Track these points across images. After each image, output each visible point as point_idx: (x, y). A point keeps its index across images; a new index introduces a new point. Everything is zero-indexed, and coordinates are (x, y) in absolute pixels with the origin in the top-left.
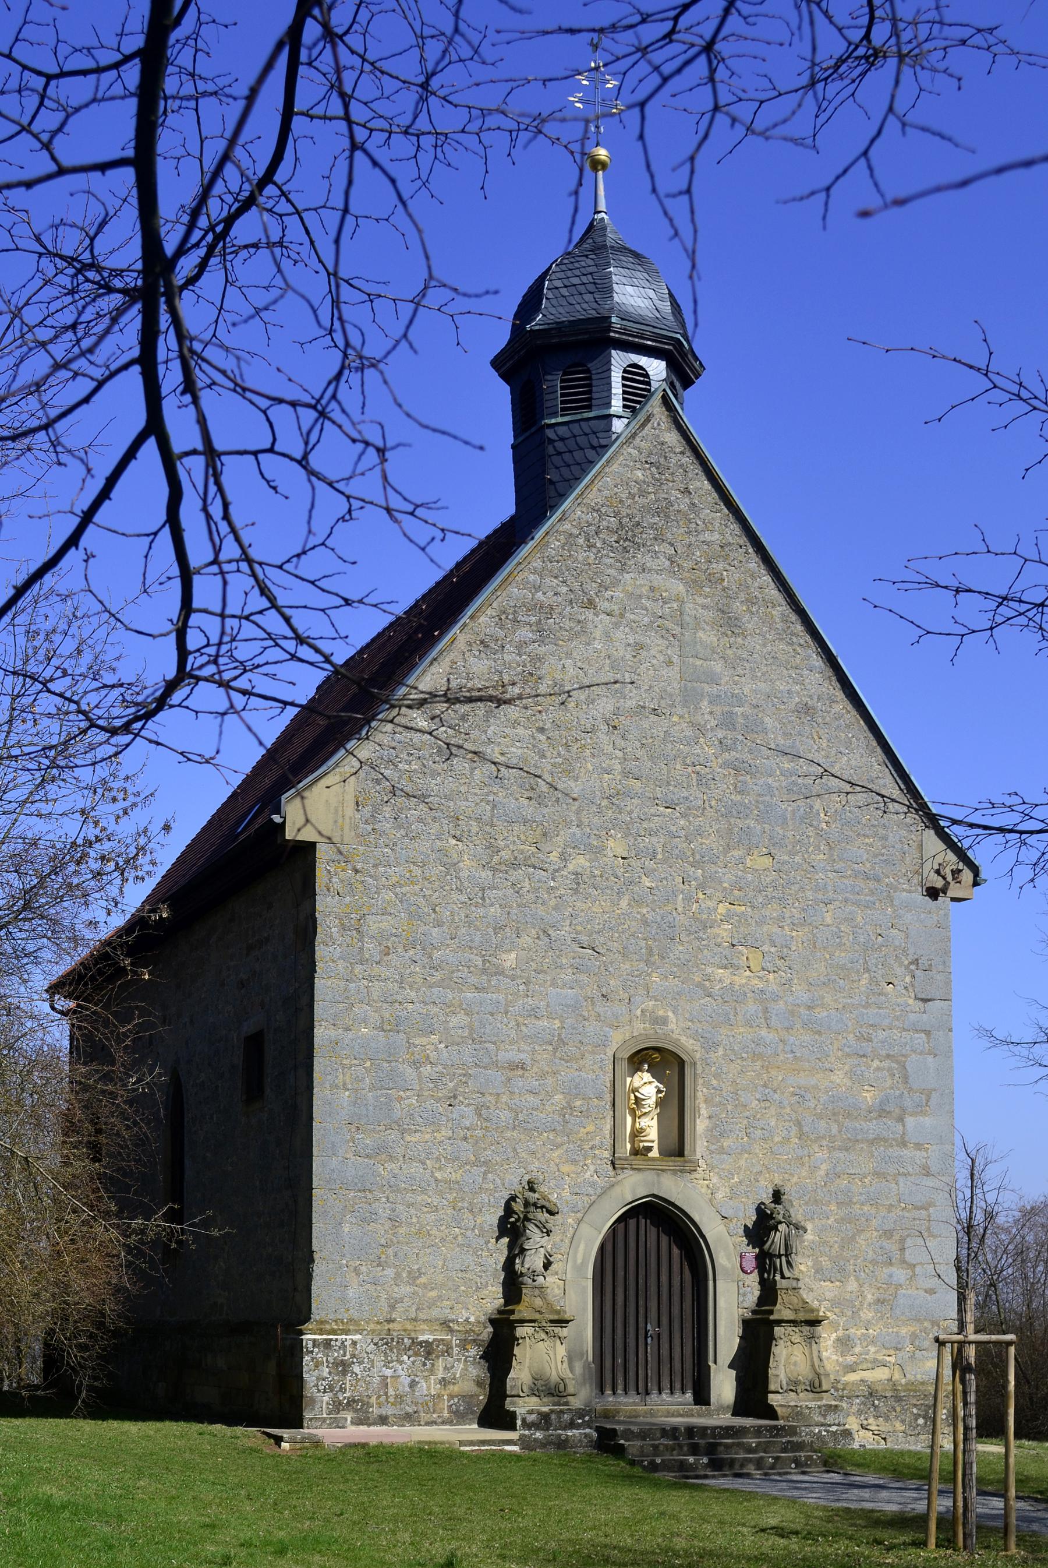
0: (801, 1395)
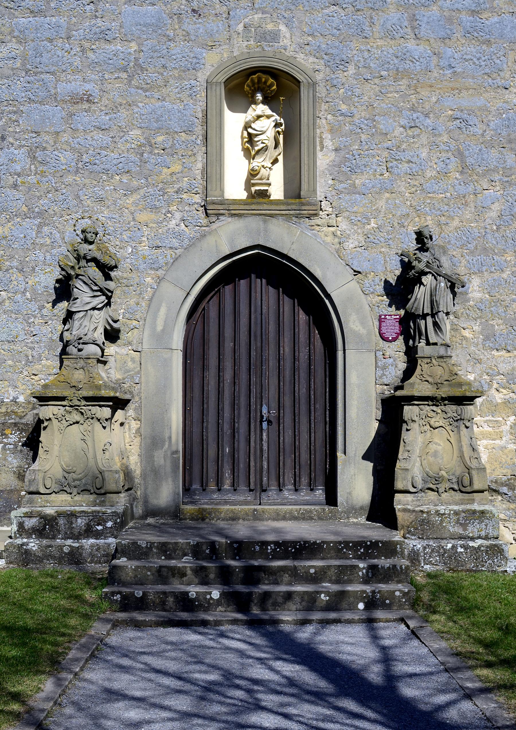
0: (444, 495)
